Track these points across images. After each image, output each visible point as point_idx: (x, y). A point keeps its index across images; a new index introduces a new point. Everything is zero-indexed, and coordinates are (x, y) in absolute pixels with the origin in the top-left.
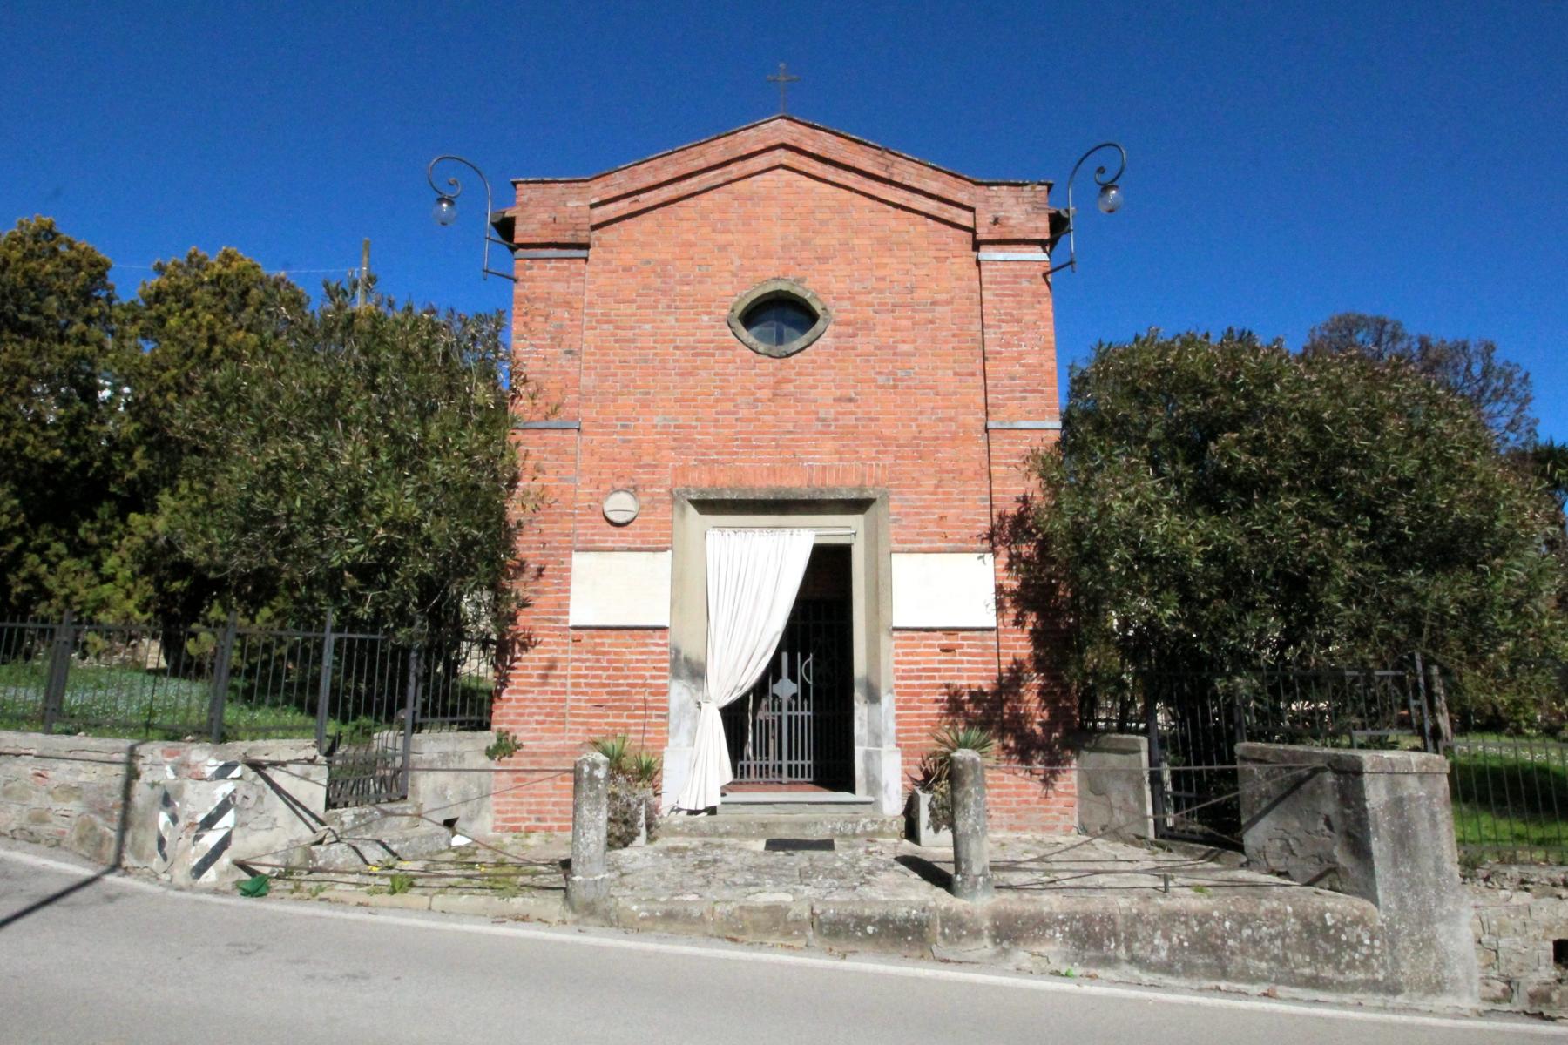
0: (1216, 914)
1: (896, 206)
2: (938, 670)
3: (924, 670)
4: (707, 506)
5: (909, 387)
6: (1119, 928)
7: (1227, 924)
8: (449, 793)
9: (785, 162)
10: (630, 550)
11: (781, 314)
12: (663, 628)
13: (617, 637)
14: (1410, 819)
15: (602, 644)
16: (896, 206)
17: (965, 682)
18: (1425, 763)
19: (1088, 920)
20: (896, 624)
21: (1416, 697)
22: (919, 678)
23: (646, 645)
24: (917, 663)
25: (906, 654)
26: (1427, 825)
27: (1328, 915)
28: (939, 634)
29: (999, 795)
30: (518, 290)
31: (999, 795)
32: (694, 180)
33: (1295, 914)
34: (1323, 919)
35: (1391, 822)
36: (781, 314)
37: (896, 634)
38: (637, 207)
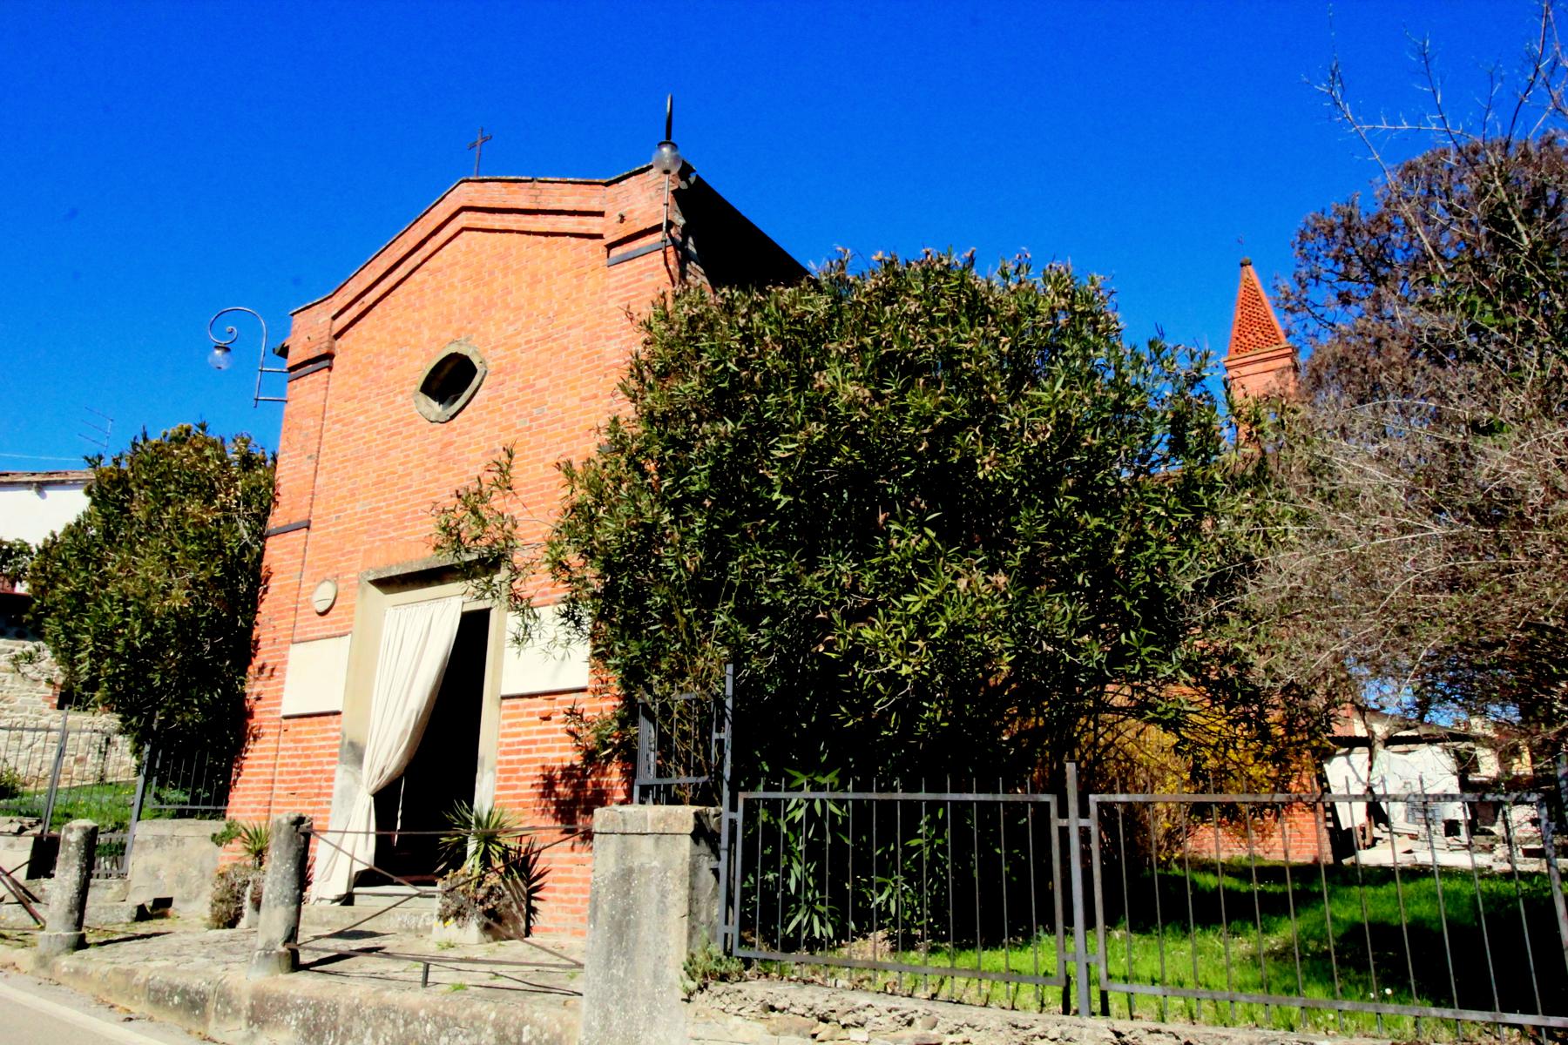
0: (422, 1013)
1: (546, 234)
2: (534, 742)
3: (524, 743)
4: (388, 584)
5: (541, 426)
6: (341, 1020)
7: (429, 1027)
8: (162, 873)
9: (465, 224)
10: (328, 637)
11: (451, 379)
12: (338, 713)
13: (311, 724)
14: (634, 899)
15: (300, 733)
16: (546, 234)
17: (557, 755)
18: (663, 819)
19: (318, 1007)
20: (504, 693)
21: (719, 731)
22: (518, 752)
23: (326, 731)
24: (518, 735)
25: (512, 725)
26: (654, 907)
27: (526, 1029)
28: (540, 699)
29: (567, 891)
30: (288, 409)
31: (567, 891)
32: (402, 267)
33: (495, 1025)
34: (519, 1033)
35: (613, 906)
36: (451, 379)
37: (505, 703)
38: (363, 308)
